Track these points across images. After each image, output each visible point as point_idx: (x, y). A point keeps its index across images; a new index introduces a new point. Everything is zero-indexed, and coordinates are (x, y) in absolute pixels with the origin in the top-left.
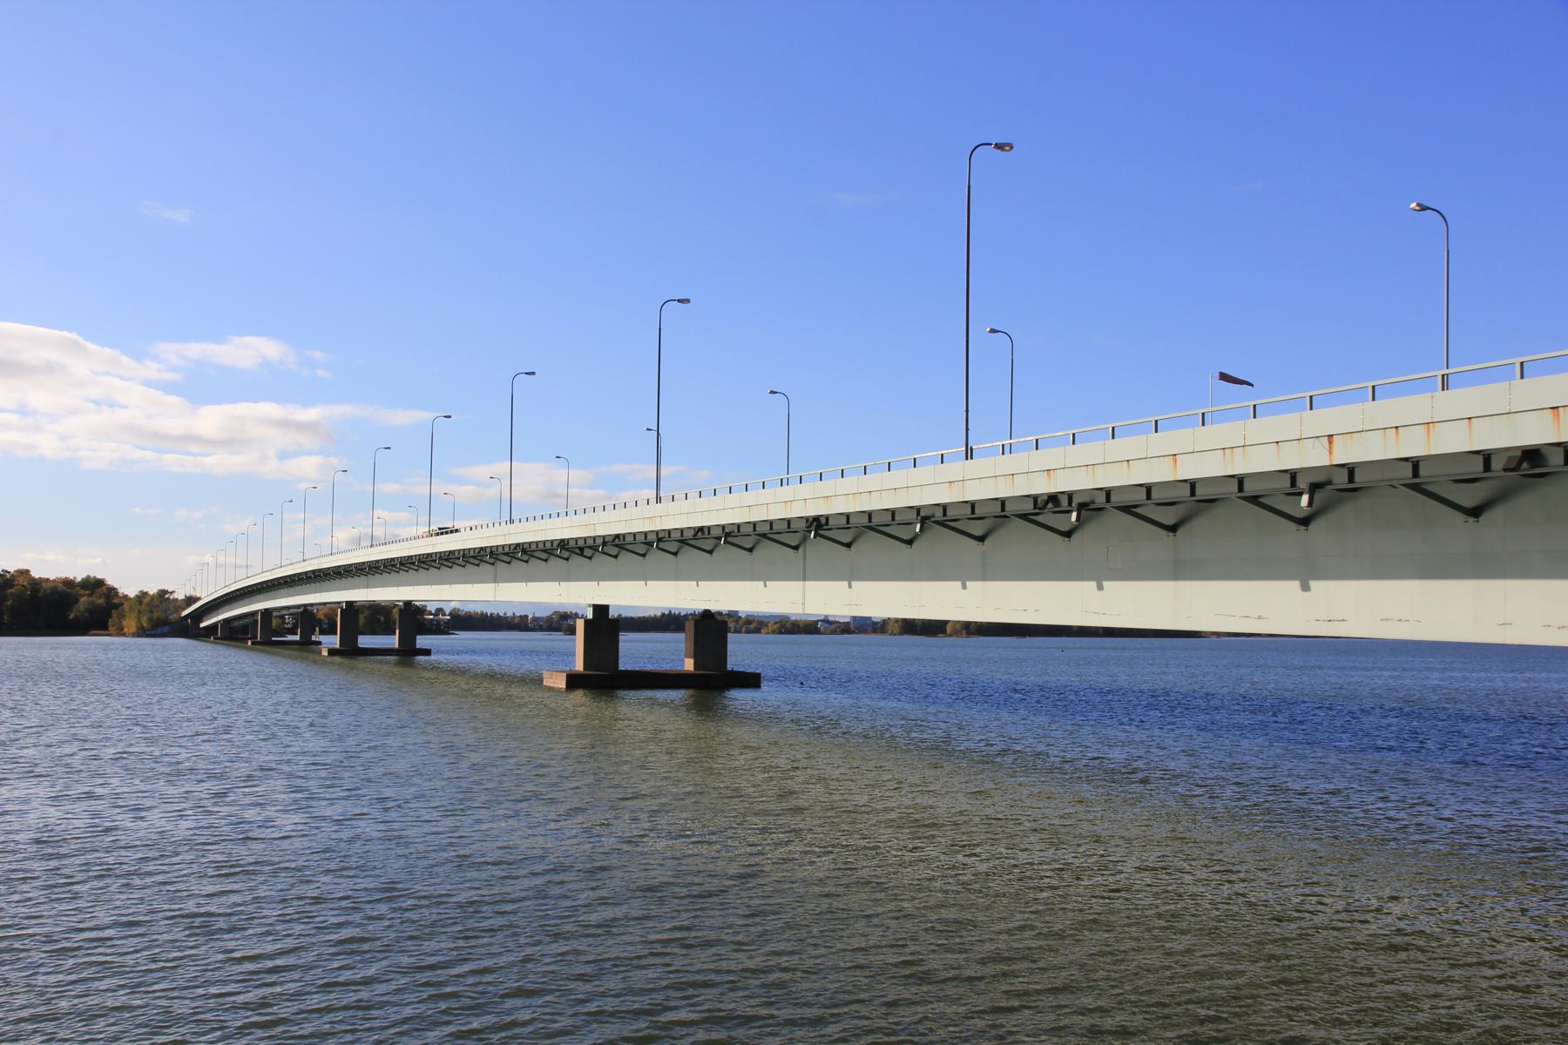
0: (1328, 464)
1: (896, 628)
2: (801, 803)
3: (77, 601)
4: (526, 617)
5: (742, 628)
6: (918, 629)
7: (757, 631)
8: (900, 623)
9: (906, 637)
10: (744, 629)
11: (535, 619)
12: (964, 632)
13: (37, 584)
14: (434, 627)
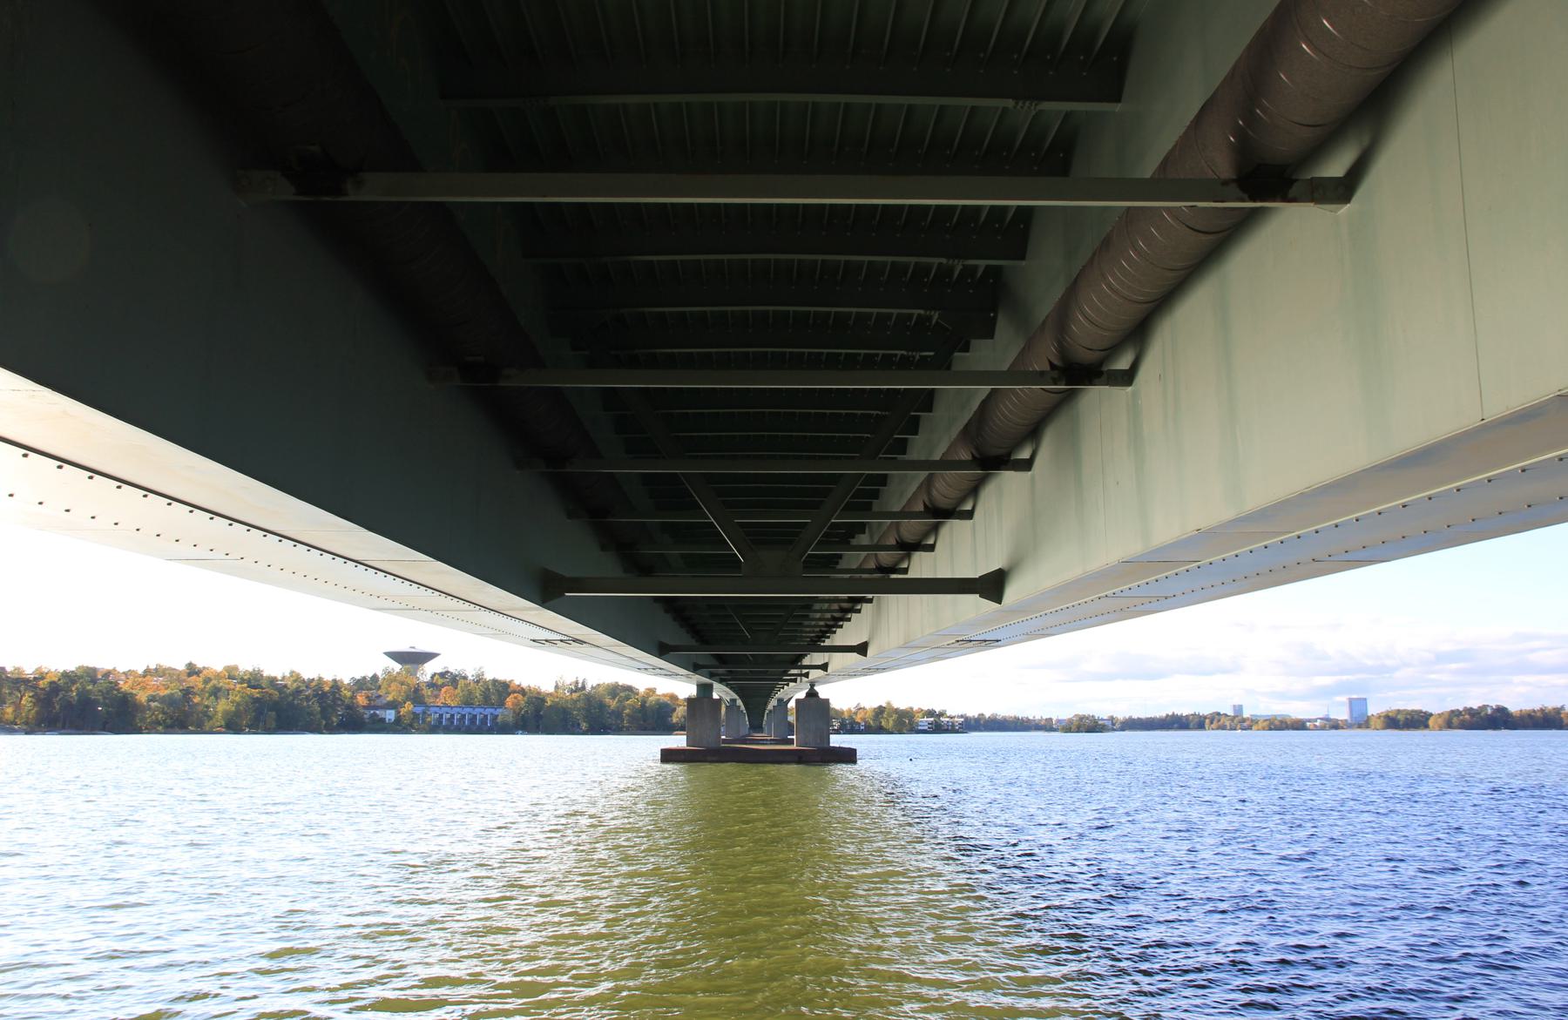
0: (1229, 514)
1: (1379, 723)
2: (1104, 874)
3: (674, 710)
4: (1051, 719)
5: (1237, 725)
6: (1401, 723)
7: (1250, 728)
8: (1382, 718)
9: (1389, 732)
10: (1239, 726)
11: (1059, 721)
12: (510, 690)
13: (1134, 720)
14: (950, 728)
